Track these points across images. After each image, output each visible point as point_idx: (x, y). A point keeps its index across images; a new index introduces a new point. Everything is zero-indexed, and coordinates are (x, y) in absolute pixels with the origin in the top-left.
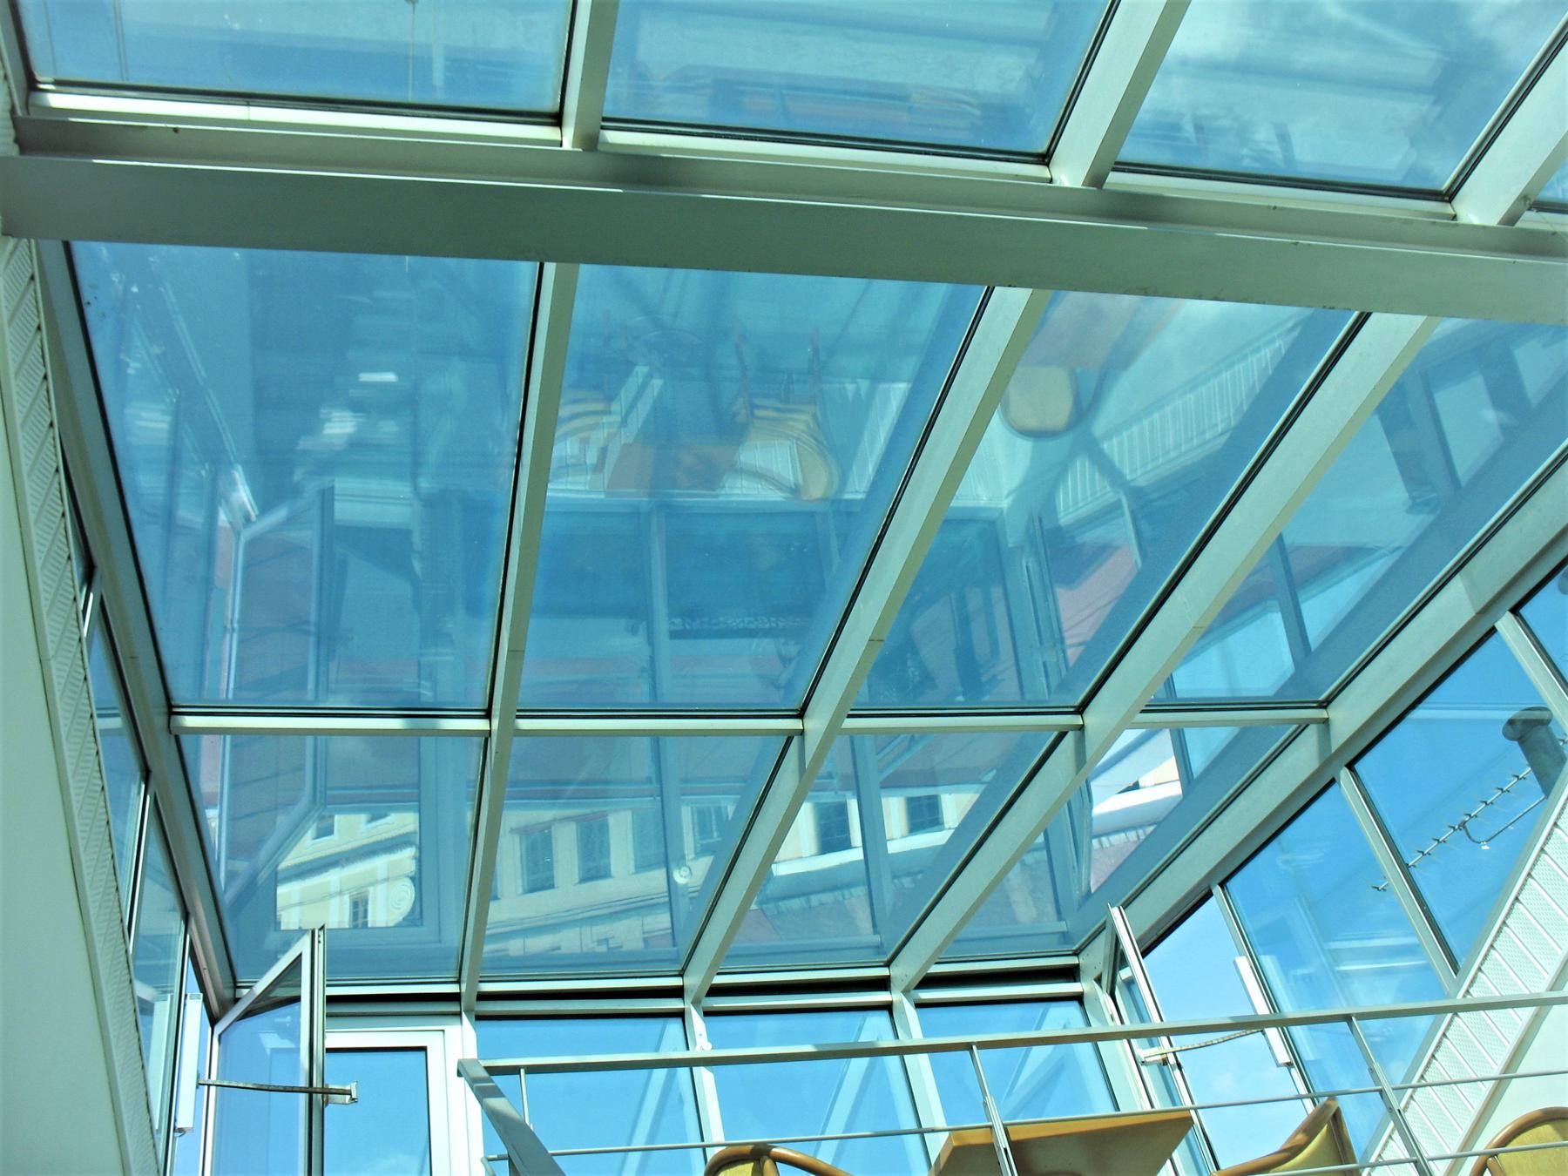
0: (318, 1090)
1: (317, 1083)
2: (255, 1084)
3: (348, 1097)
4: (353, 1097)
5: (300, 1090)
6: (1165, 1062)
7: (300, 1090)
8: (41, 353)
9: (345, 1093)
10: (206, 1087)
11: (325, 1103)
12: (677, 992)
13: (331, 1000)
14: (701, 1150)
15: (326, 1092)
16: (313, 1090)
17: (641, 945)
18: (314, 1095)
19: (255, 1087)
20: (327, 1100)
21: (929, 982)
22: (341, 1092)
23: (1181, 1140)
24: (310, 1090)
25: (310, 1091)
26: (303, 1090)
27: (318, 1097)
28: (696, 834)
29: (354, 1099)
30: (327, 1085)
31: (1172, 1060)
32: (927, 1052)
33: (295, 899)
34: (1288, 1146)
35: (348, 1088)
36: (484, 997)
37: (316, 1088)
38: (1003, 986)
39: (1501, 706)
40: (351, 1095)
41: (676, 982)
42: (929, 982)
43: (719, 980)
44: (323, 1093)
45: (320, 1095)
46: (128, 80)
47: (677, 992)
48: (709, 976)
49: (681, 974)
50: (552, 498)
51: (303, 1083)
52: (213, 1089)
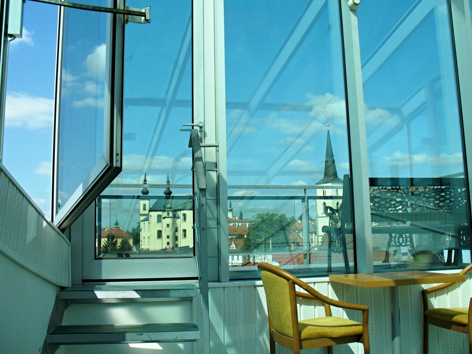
0: (121, 11)
1: (120, 5)
2: (71, 3)
3: (143, 18)
4: (148, 18)
5: (106, 10)
7: (106, 10)
10: (59, 6)
16: (117, 11)
17: (468, 223)
18: (118, 15)
19: (71, 5)
20: (127, 20)
22: (138, 14)
23: (45, 227)
24: (114, 10)
25: (114, 11)
26: (109, 10)
28: (391, 295)
29: (148, 20)
30: (128, 7)
34: (362, 338)
35: (143, 11)
37: (119, 9)
38: (345, 95)
39: (199, 266)
40: (145, 16)
44: (124, 14)
45: (122, 15)
46: (321, 290)
50: (325, 263)
52: (62, 7)
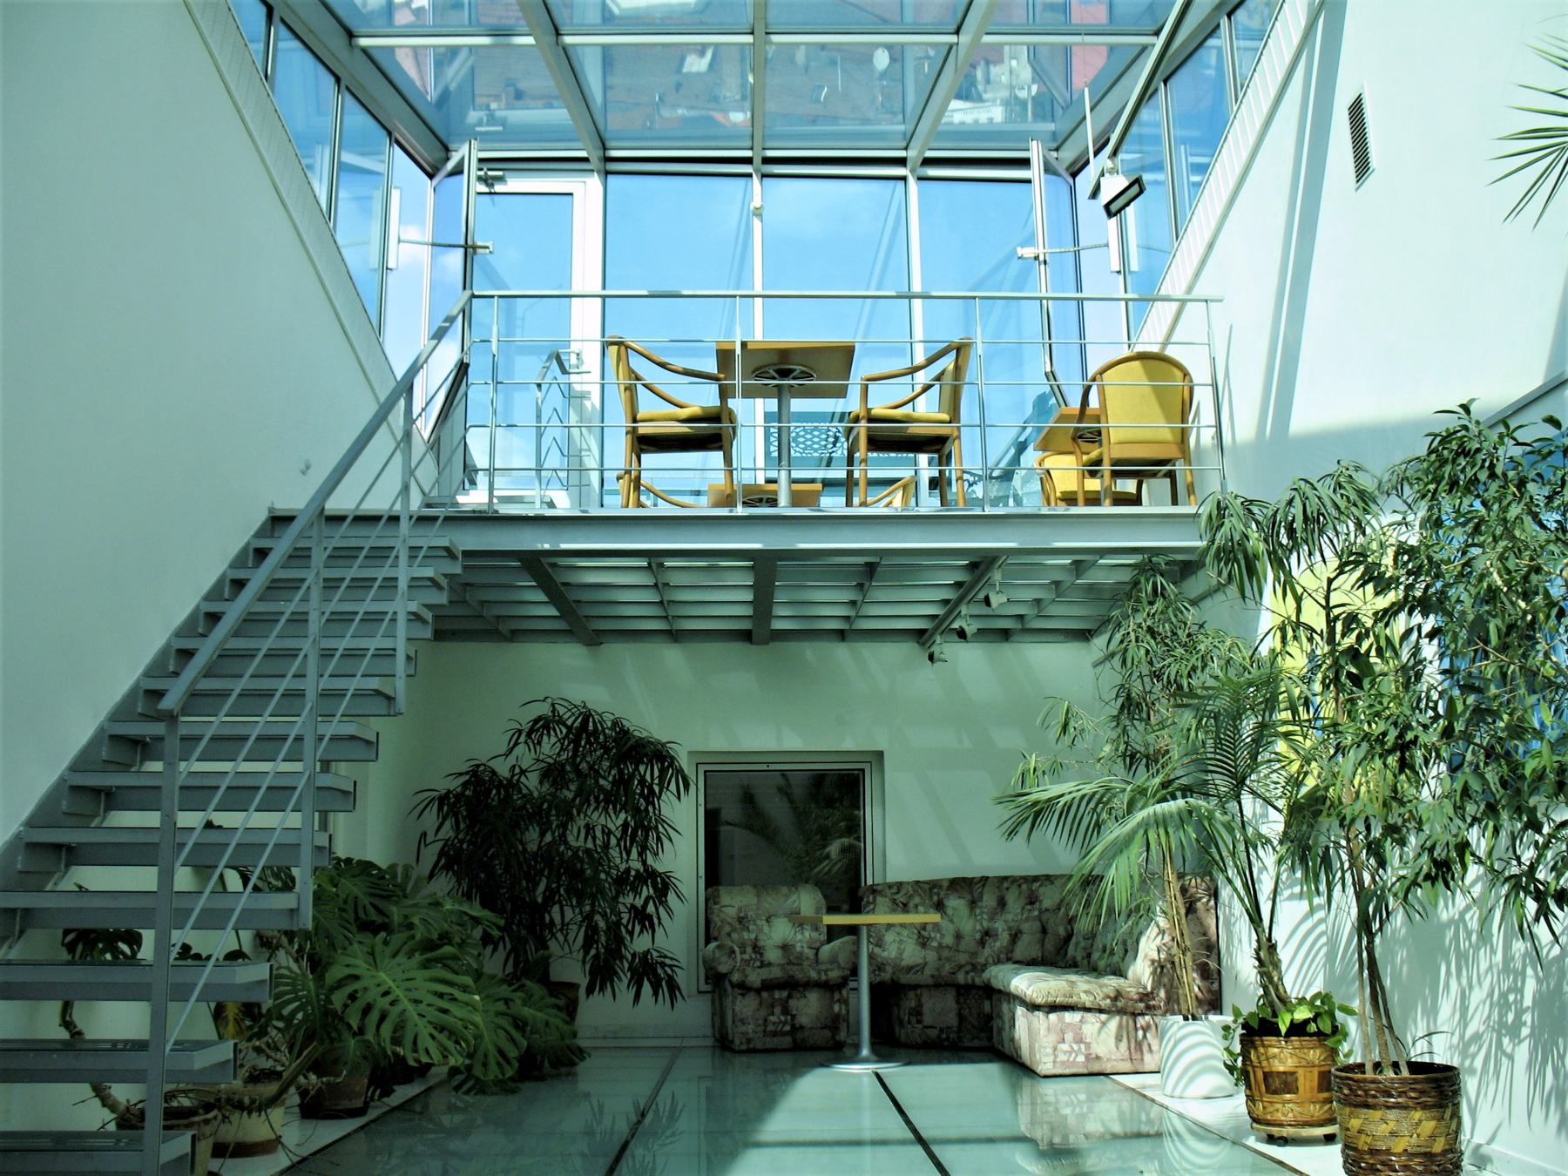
1: (470, 242)
6: (1037, 258)
8: (659, 388)
9: (487, 247)
11: (475, 253)
12: (901, 162)
13: (481, 160)
14: (599, 300)
15: (475, 248)
21: (928, 162)
25: (466, 247)
27: (470, 251)
31: (1042, 258)
32: (234, 985)
33: (1368, 476)
36: (767, 161)
41: (902, 154)
42: (928, 162)
43: (930, 154)
47: (901, 162)
48: (922, 151)
49: (906, 149)
51: (463, 243)
